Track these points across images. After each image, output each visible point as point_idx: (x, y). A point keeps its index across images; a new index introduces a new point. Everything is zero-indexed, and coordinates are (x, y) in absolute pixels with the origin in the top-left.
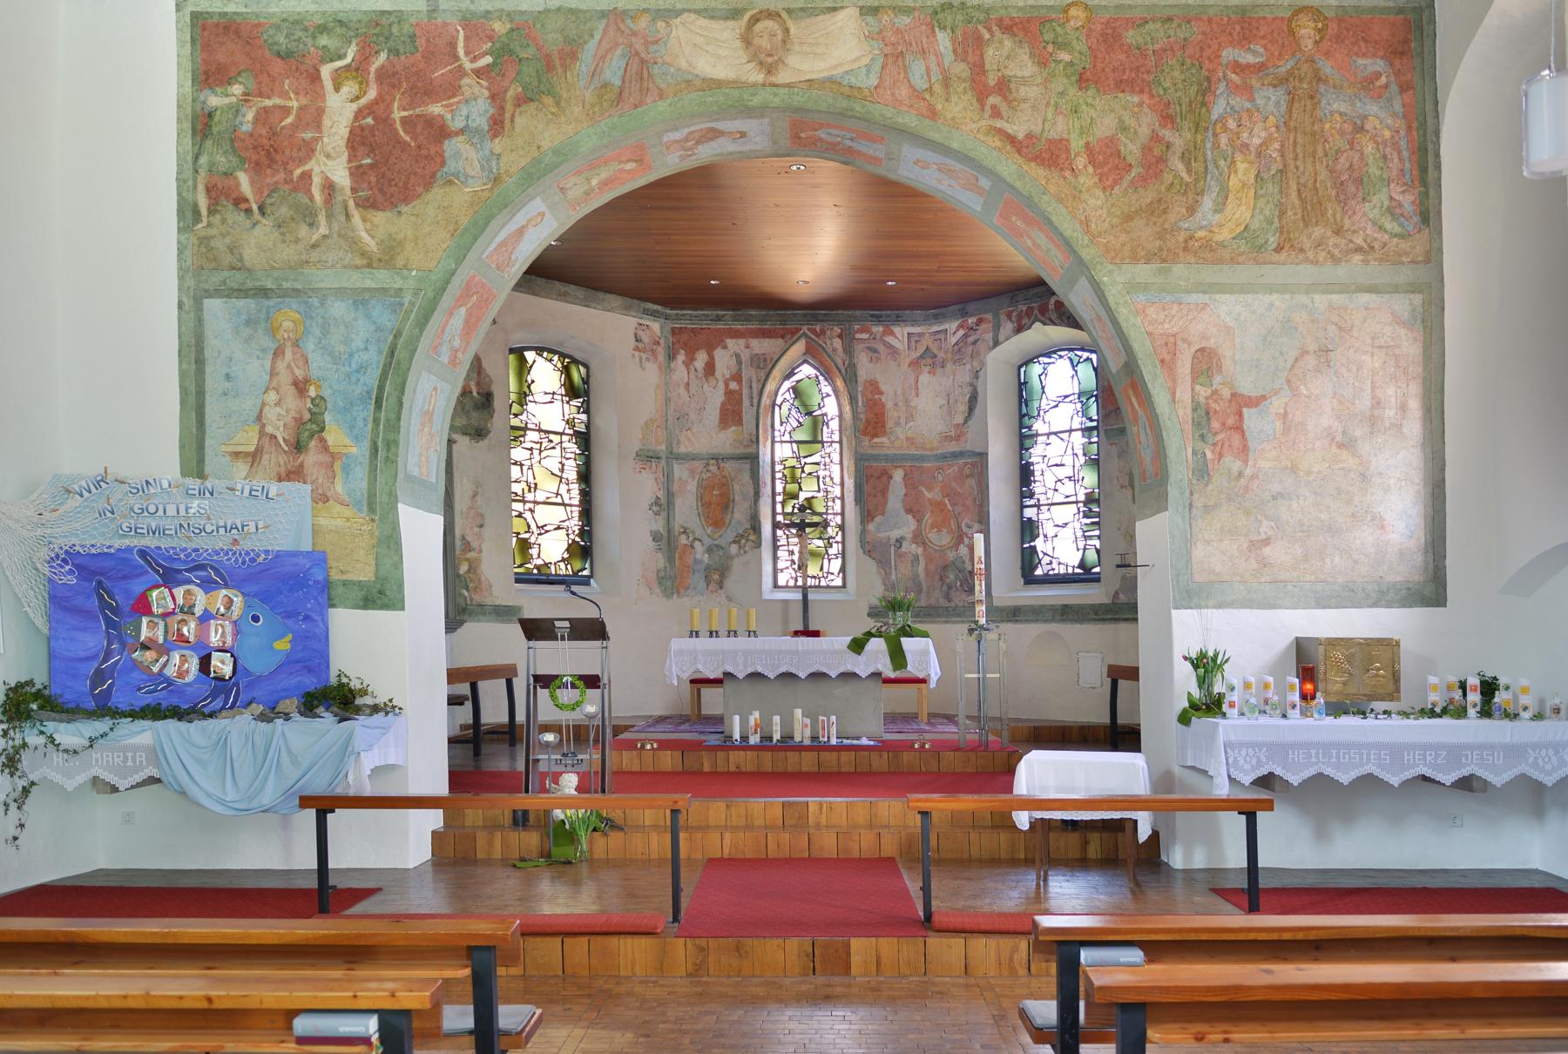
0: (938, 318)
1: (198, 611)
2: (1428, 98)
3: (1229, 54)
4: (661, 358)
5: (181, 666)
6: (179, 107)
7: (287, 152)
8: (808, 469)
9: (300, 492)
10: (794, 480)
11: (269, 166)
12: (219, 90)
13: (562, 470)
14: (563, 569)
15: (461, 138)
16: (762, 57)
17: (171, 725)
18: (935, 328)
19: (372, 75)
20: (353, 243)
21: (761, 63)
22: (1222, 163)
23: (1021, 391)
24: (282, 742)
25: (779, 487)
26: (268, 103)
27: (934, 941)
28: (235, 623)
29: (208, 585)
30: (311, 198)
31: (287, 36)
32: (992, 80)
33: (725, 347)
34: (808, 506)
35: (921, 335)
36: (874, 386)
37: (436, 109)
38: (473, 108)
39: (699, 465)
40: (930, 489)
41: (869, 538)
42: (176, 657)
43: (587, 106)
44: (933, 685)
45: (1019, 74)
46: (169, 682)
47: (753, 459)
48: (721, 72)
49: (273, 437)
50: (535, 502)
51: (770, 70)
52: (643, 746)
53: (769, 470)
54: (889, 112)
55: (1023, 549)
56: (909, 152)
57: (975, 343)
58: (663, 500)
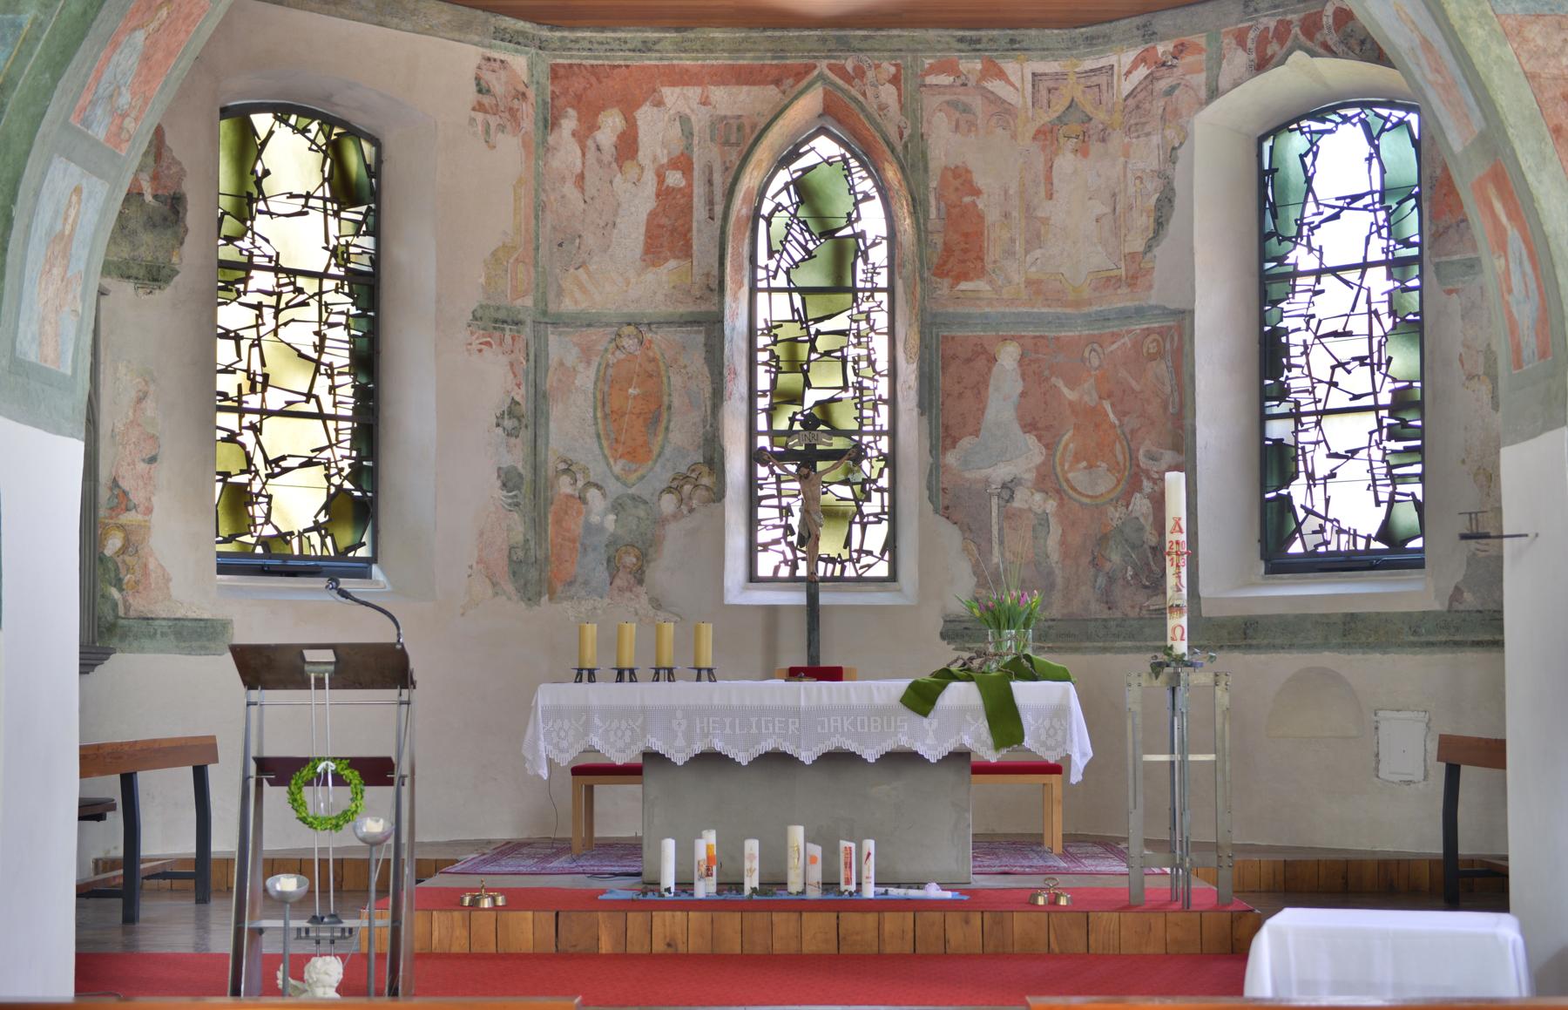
4: (528, 123)
8: (822, 344)
13: (320, 348)
23: (1262, 187)
25: (763, 382)
33: (659, 103)
35: (1060, 77)
36: (961, 178)
39: (599, 338)
40: (1072, 384)
44: (1076, 777)
47: (713, 324)
50: (265, 413)
52: (475, 903)
53: (744, 345)
55: (1264, 503)
57: (1170, 92)
58: (526, 407)
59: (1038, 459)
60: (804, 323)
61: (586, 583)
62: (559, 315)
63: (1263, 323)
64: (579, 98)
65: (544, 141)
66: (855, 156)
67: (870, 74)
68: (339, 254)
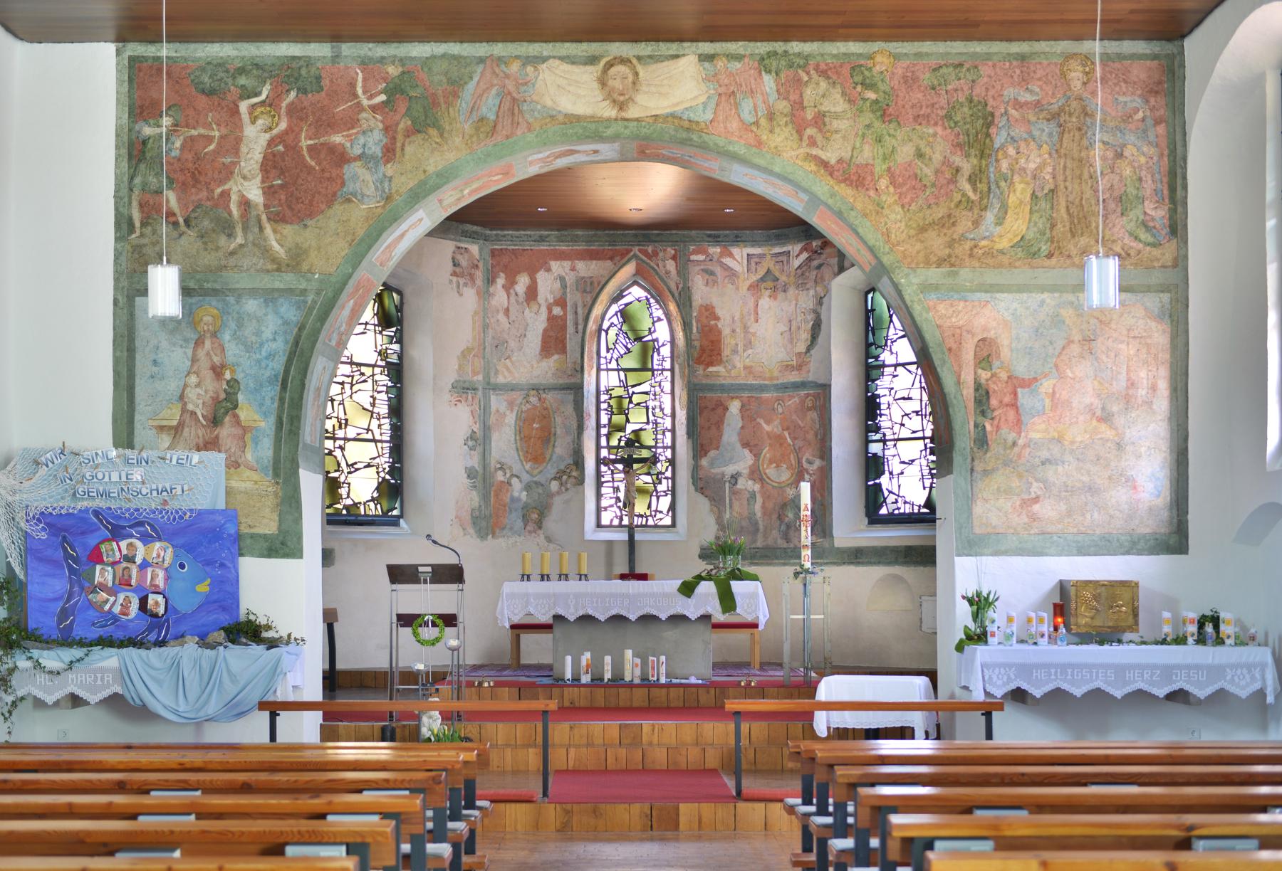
0: (780, 239)
1: (139, 560)
2: (1178, 130)
4: (479, 282)
5: (124, 605)
6: (117, 135)
7: (210, 174)
8: (636, 399)
9: (216, 459)
11: (194, 186)
12: (152, 122)
13: (373, 405)
14: (373, 509)
15: (358, 163)
16: (615, 96)
18: (777, 250)
19: (283, 110)
20: (266, 251)
21: (614, 101)
22: (1003, 184)
23: (867, 319)
24: (223, 665)
25: (604, 419)
26: (194, 132)
27: (742, 806)
28: (166, 569)
30: (230, 213)
31: (211, 77)
32: (809, 115)
33: (549, 270)
34: (634, 441)
35: (762, 256)
36: (709, 311)
37: (337, 139)
39: (518, 396)
40: (768, 422)
41: (701, 474)
42: (121, 597)
43: (467, 137)
44: (761, 627)
45: (833, 110)
46: (115, 619)
47: (578, 389)
48: (581, 109)
49: (193, 413)
50: (346, 439)
51: (622, 106)
52: (480, 684)
53: (594, 400)
55: (868, 487)
56: (736, 167)
57: (819, 267)
58: (479, 434)
59: (750, 462)
60: (626, 387)
61: (511, 529)
62: (496, 384)
63: (867, 391)
64: (506, 267)
65: (488, 291)
66: (653, 297)
67: (661, 254)
68: (382, 354)
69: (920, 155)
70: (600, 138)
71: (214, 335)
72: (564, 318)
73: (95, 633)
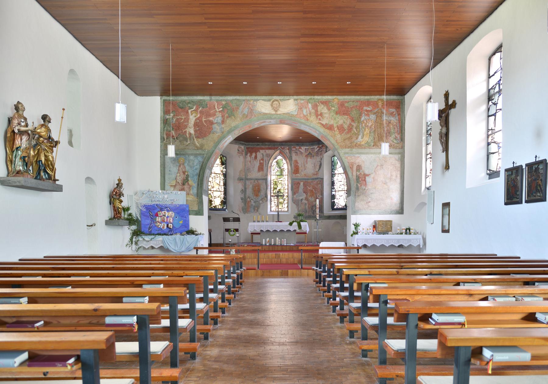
0: (312, 145)
3: (365, 108)
5: (163, 226)
9: (184, 193)
10: (276, 184)
14: (220, 207)
17: (165, 236)
20: (195, 145)
25: (272, 186)
29: (168, 211)
32: (319, 113)
34: (279, 191)
36: (296, 162)
37: (211, 119)
38: (218, 118)
42: (163, 224)
46: (161, 229)
47: (266, 179)
48: (267, 112)
54: (299, 119)
56: (302, 125)
68: (222, 171)
69: (344, 122)
70: (271, 119)
71: (183, 164)
72: (263, 163)
73: (157, 232)
